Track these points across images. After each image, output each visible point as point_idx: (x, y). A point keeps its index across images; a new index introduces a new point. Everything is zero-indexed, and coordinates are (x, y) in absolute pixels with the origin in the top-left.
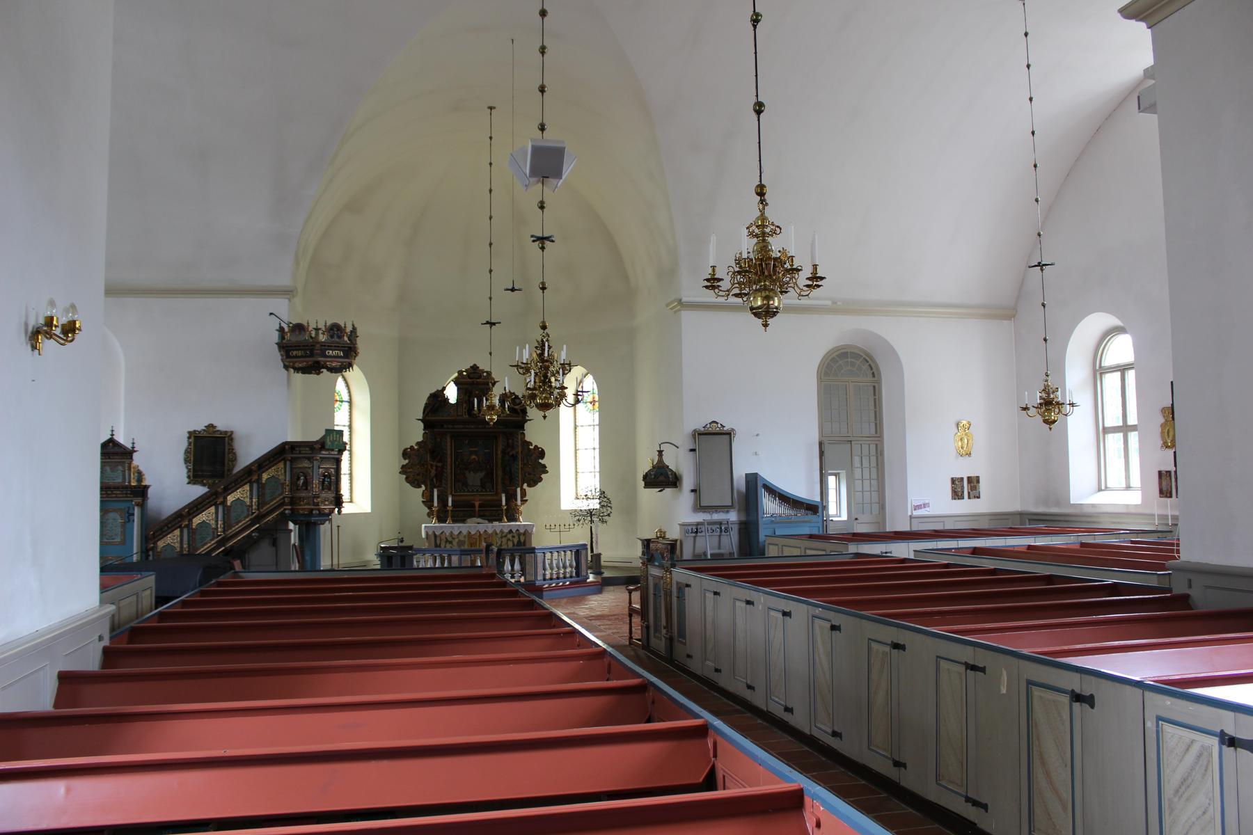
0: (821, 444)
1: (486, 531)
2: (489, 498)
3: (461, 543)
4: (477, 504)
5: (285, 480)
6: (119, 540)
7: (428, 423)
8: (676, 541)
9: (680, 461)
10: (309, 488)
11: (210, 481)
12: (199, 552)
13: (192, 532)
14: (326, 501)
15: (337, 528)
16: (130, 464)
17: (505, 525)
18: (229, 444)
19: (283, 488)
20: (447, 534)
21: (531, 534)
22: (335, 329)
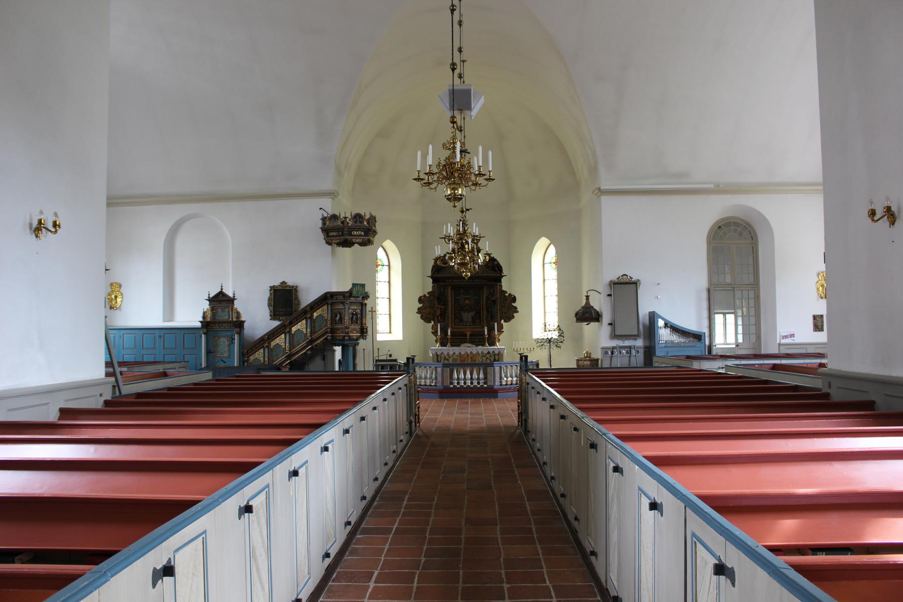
0: (709, 290)
1: (471, 352)
2: (477, 330)
3: (454, 360)
4: (468, 334)
5: (328, 317)
6: (227, 355)
7: (435, 280)
8: (598, 360)
9: (599, 303)
10: (343, 322)
11: (284, 318)
12: (275, 363)
13: (271, 351)
14: (354, 330)
15: (377, 350)
16: (233, 307)
17: (488, 348)
18: (295, 294)
19: (327, 322)
20: (445, 354)
21: (502, 355)
22: (358, 217)
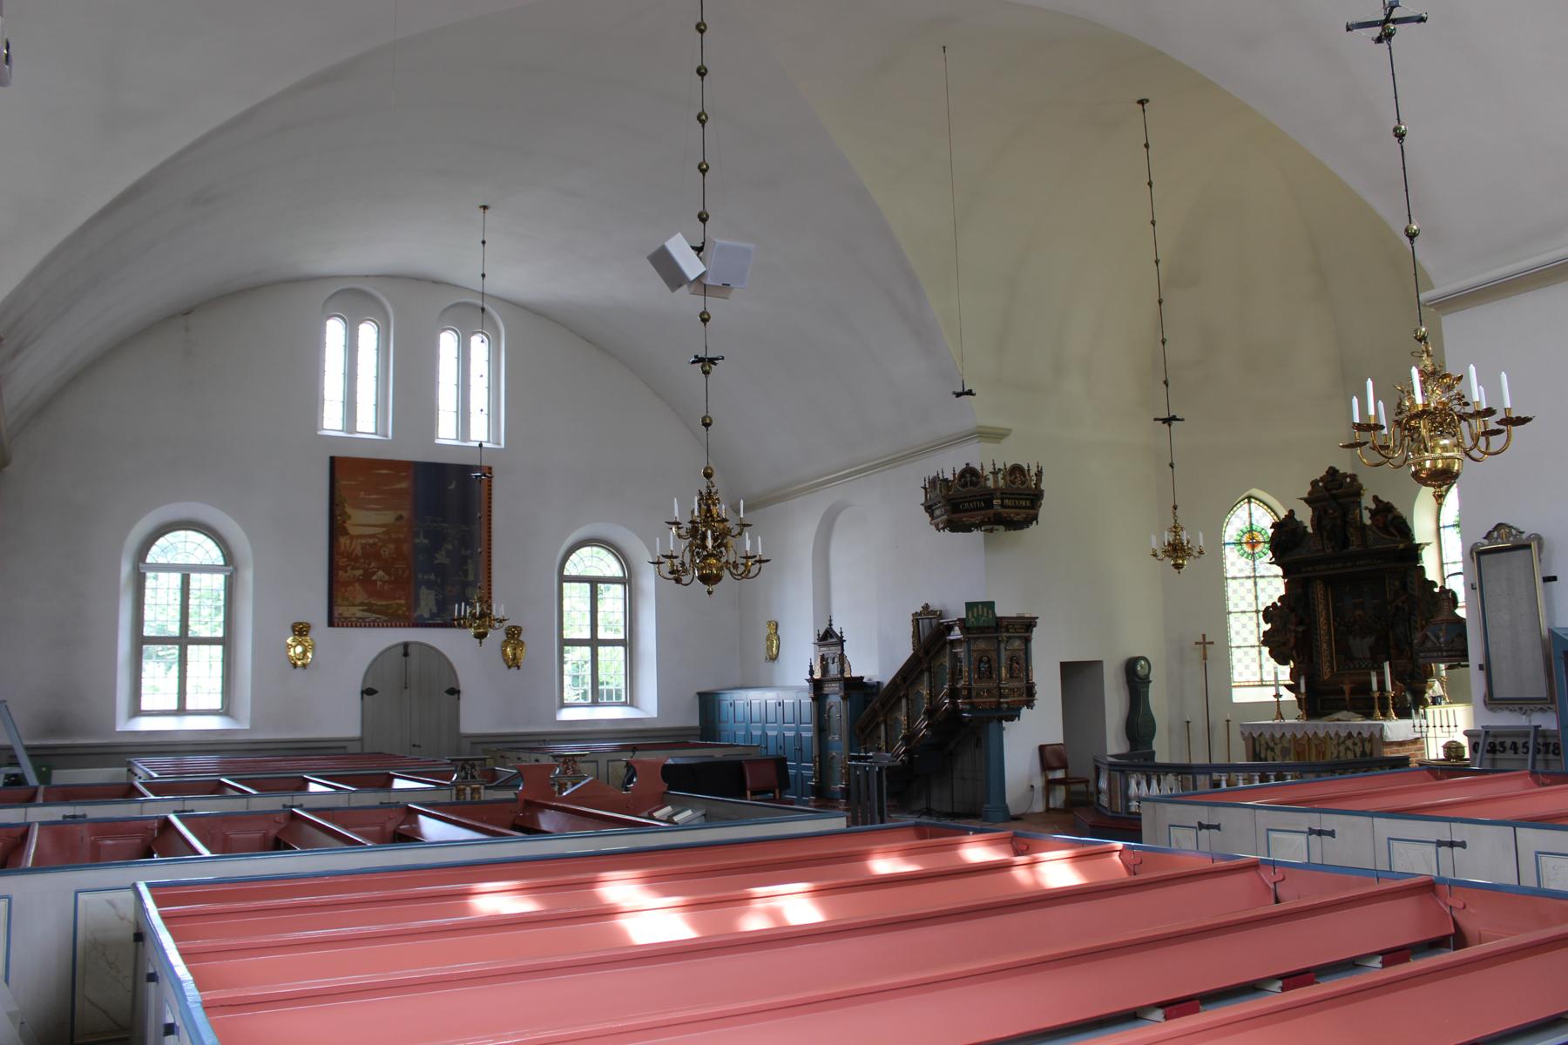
4: (1347, 688)
22: (968, 475)
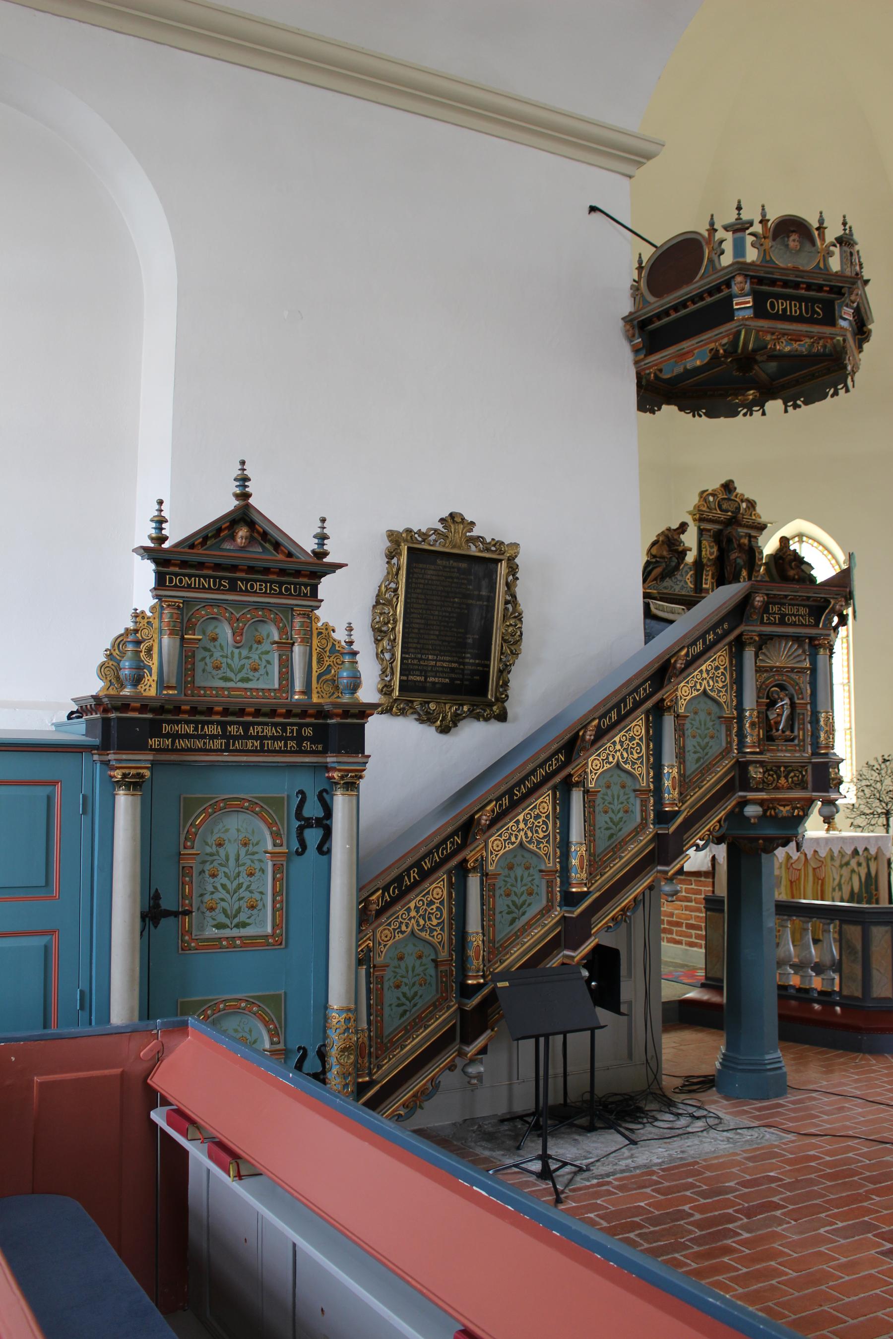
16: (309, 616)
